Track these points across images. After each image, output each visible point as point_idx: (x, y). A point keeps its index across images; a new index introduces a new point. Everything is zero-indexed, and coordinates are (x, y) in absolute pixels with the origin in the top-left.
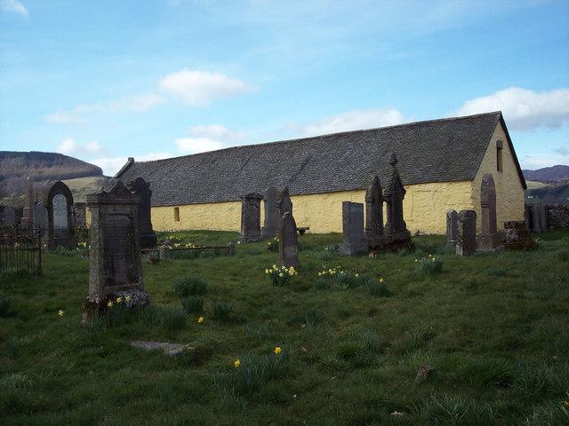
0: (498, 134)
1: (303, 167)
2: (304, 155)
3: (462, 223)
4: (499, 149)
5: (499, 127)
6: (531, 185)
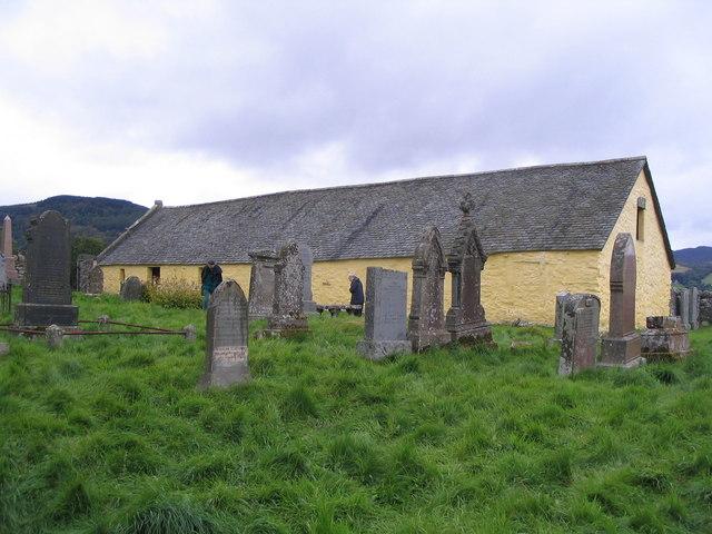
0: (639, 189)
1: (368, 222)
2: (374, 205)
3: (573, 311)
4: (640, 210)
5: (641, 178)
6: (680, 269)
